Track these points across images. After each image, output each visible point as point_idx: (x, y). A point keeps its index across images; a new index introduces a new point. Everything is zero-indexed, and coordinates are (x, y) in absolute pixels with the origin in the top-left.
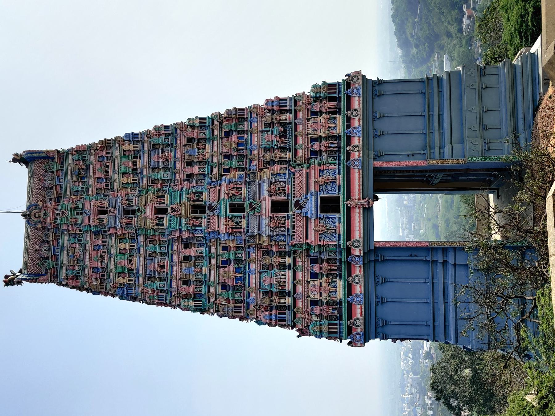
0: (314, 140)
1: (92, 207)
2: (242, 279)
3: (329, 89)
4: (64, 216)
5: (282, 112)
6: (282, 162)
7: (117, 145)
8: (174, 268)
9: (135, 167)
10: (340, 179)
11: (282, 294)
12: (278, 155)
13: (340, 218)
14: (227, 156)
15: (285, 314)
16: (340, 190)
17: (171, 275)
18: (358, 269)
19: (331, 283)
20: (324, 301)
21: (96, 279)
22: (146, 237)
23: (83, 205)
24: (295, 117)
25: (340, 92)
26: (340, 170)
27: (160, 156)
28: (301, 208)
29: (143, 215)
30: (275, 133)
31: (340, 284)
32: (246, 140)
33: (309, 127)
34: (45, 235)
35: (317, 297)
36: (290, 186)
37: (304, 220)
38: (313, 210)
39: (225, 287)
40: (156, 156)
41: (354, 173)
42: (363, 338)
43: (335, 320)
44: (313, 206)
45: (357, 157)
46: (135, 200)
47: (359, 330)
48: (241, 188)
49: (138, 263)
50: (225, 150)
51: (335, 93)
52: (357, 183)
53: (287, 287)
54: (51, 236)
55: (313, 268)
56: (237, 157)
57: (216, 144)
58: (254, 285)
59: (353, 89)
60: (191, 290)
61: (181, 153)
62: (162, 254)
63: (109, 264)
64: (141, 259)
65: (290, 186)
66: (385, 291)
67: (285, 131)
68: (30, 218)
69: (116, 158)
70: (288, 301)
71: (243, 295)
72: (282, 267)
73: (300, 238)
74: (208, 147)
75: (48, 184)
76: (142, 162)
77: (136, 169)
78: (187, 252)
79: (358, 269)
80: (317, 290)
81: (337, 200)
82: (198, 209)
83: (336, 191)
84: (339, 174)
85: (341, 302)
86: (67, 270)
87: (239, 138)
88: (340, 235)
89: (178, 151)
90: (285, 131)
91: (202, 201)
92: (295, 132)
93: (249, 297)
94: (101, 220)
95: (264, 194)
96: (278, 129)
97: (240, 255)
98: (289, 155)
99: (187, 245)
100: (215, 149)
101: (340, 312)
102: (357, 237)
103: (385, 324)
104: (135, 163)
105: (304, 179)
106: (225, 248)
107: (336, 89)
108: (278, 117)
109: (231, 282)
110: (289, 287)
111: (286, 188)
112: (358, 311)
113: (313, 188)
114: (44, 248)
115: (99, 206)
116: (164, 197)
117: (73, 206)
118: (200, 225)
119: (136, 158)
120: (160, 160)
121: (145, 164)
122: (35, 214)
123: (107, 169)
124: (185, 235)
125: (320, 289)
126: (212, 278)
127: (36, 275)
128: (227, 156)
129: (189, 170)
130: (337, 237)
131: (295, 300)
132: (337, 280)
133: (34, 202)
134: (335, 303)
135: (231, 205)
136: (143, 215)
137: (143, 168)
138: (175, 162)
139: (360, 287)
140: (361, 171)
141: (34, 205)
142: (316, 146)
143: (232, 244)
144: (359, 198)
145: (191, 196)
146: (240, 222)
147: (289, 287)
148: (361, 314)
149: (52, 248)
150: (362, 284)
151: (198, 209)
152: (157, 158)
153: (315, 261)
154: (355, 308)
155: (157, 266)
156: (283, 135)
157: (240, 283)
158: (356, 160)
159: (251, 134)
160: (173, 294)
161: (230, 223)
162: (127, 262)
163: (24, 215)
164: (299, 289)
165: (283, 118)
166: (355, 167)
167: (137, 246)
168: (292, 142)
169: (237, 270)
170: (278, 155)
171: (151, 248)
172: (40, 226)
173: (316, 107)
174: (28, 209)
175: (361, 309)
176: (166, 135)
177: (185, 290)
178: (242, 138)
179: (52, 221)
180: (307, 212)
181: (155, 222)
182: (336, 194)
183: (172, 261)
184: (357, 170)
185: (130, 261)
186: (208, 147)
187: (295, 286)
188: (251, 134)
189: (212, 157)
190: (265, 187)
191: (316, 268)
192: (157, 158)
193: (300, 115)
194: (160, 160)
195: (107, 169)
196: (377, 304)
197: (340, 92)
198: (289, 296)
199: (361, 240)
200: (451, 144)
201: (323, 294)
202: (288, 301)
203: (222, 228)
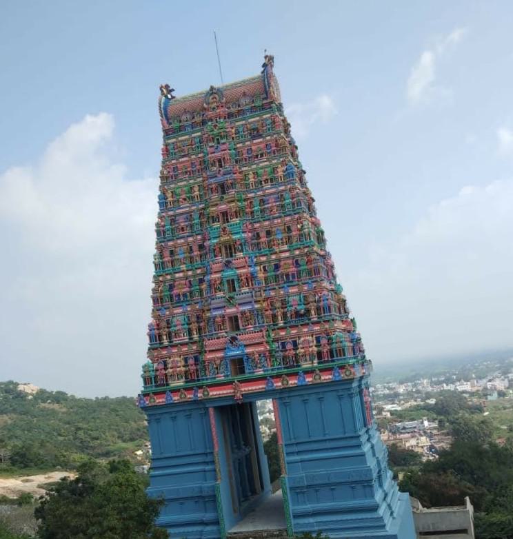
0: (295, 344)
1: (223, 152)
2: (289, 279)
3: (340, 350)
4: (213, 127)
5: (318, 309)
6: (274, 317)
7: (281, 159)
8: (182, 241)
9: (263, 183)
10: (260, 372)
11: (169, 335)
12: (279, 313)
13: (227, 376)
14: (277, 267)
15: (156, 341)
16: (250, 373)
17: (178, 239)
18: (310, 379)
19: (179, 376)
20: (298, 352)
21: (169, 172)
22: (204, 209)
23: (224, 143)
24: (314, 323)
25: (338, 360)
26: (267, 370)
27: (274, 204)
28: (231, 343)
29: (218, 202)
30: (299, 308)
31: (181, 383)
32: (292, 282)
33: (307, 339)
34: (235, 103)
35: (170, 366)
36: (224, 334)
37: (221, 347)
38: (230, 354)
39: (171, 287)
40: (273, 200)
41: (261, 384)
42: (142, 406)
43: (155, 382)
44: (236, 352)
45: (307, 380)
46: (232, 192)
47: (147, 402)
48: (248, 286)
49: (185, 207)
50: (282, 263)
51: (337, 356)
52: (254, 388)
53: (175, 339)
54: (198, 119)
55: (191, 359)
56: (279, 276)
57: (287, 254)
58: (175, 312)
59: (339, 372)
60: (167, 259)
61: (278, 223)
62: (192, 226)
63: (182, 180)
64: (187, 209)
65: (252, 329)
66: (181, 420)
67: (302, 316)
68: (212, 94)
69: (270, 161)
70: (166, 342)
71: (168, 304)
72: (190, 332)
73: (210, 344)
74: (286, 247)
75: (184, 118)
76: (269, 189)
77: (261, 184)
78: (195, 248)
79: (310, 379)
80: (305, 345)
81: (242, 371)
82: (231, 249)
83: (250, 370)
84: (224, 376)
85: (168, 385)
86: (242, 125)
87: (293, 275)
88: (215, 378)
89: (279, 220)
90: (302, 316)
91: (235, 253)
92: (301, 325)
93: (166, 309)
94: (213, 165)
95: (242, 308)
96: (302, 309)
97: (197, 295)
98: (281, 324)
99: (201, 247)
100: (283, 255)
101: (160, 385)
102: (211, 394)
103: (158, 421)
104: (266, 181)
105: (257, 341)
106: (201, 281)
107: (341, 356)
108: (312, 307)
109: (175, 292)
110: (176, 341)
111: (250, 326)
112: (161, 400)
113: (248, 350)
114: (188, 116)
115: (224, 158)
116: (237, 218)
117: (222, 134)
118: (216, 256)
119: (272, 181)
120: (270, 205)
121: (267, 191)
122: (215, 98)
123: (259, 156)
124: (207, 243)
125: (307, 347)
126: (177, 275)
127: (166, 116)
128: (277, 267)
129: (263, 234)
130: (214, 376)
131: (166, 347)
132: (184, 380)
133: (224, 93)
134: (297, 361)
135: (233, 281)
136: (218, 202)
137: (263, 191)
138: (269, 219)
139: (178, 400)
140: (263, 390)
141: (222, 94)
142: (289, 346)
143: (204, 286)
144: (242, 391)
145: (238, 243)
146: (220, 291)
147: (176, 341)
148: (159, 402)
149: (189, 123)
150: (180, 401)
151: (231, 249)
152: (272, 203)
153: (196, 359)
154: (163, 398)
155: (182, 224)
156: (297, 314)
157: (175, 299)
158: (273, 385)
159: (298, 285)
160: (163, 244)
161: (218, 282)
162: (184, 196)
163: (212, 88)
164: (175, 350)
165: (313, 312)
166: (267, 384)
167: (171, 208)
168: (292, 324)
169: (184, 295)
170: (279, 313)
171: (196, 216)
172: (205, 105)
173: (324, 341)
174: (218, 89)
175: (163, 402)
176: (293, 204)
177: (167, 253)
178: (293, 277)
179: (209, 116)
180: (229, 348)
181: (214, 215)
182: (247, 371)
183: (188, 236)
184: (264, 386)
185: (185, 199)
186: (286, 247)
187: (176, 346)
188: (298, 285)
189: (276, 253)
190: (248, 307)
191: (191, 361)
192: (272, 203)
193: (317, 328)
194: (270, 205)
195: (259, 156)
196: (170, 413)
197: (338, 360)
198: (285, 323)
199: (209, 397)
200: (301, 461)
201: (302, 350)
202: (166, 342)
203: (214, 276)
